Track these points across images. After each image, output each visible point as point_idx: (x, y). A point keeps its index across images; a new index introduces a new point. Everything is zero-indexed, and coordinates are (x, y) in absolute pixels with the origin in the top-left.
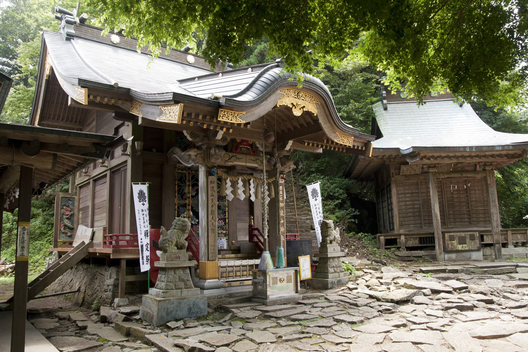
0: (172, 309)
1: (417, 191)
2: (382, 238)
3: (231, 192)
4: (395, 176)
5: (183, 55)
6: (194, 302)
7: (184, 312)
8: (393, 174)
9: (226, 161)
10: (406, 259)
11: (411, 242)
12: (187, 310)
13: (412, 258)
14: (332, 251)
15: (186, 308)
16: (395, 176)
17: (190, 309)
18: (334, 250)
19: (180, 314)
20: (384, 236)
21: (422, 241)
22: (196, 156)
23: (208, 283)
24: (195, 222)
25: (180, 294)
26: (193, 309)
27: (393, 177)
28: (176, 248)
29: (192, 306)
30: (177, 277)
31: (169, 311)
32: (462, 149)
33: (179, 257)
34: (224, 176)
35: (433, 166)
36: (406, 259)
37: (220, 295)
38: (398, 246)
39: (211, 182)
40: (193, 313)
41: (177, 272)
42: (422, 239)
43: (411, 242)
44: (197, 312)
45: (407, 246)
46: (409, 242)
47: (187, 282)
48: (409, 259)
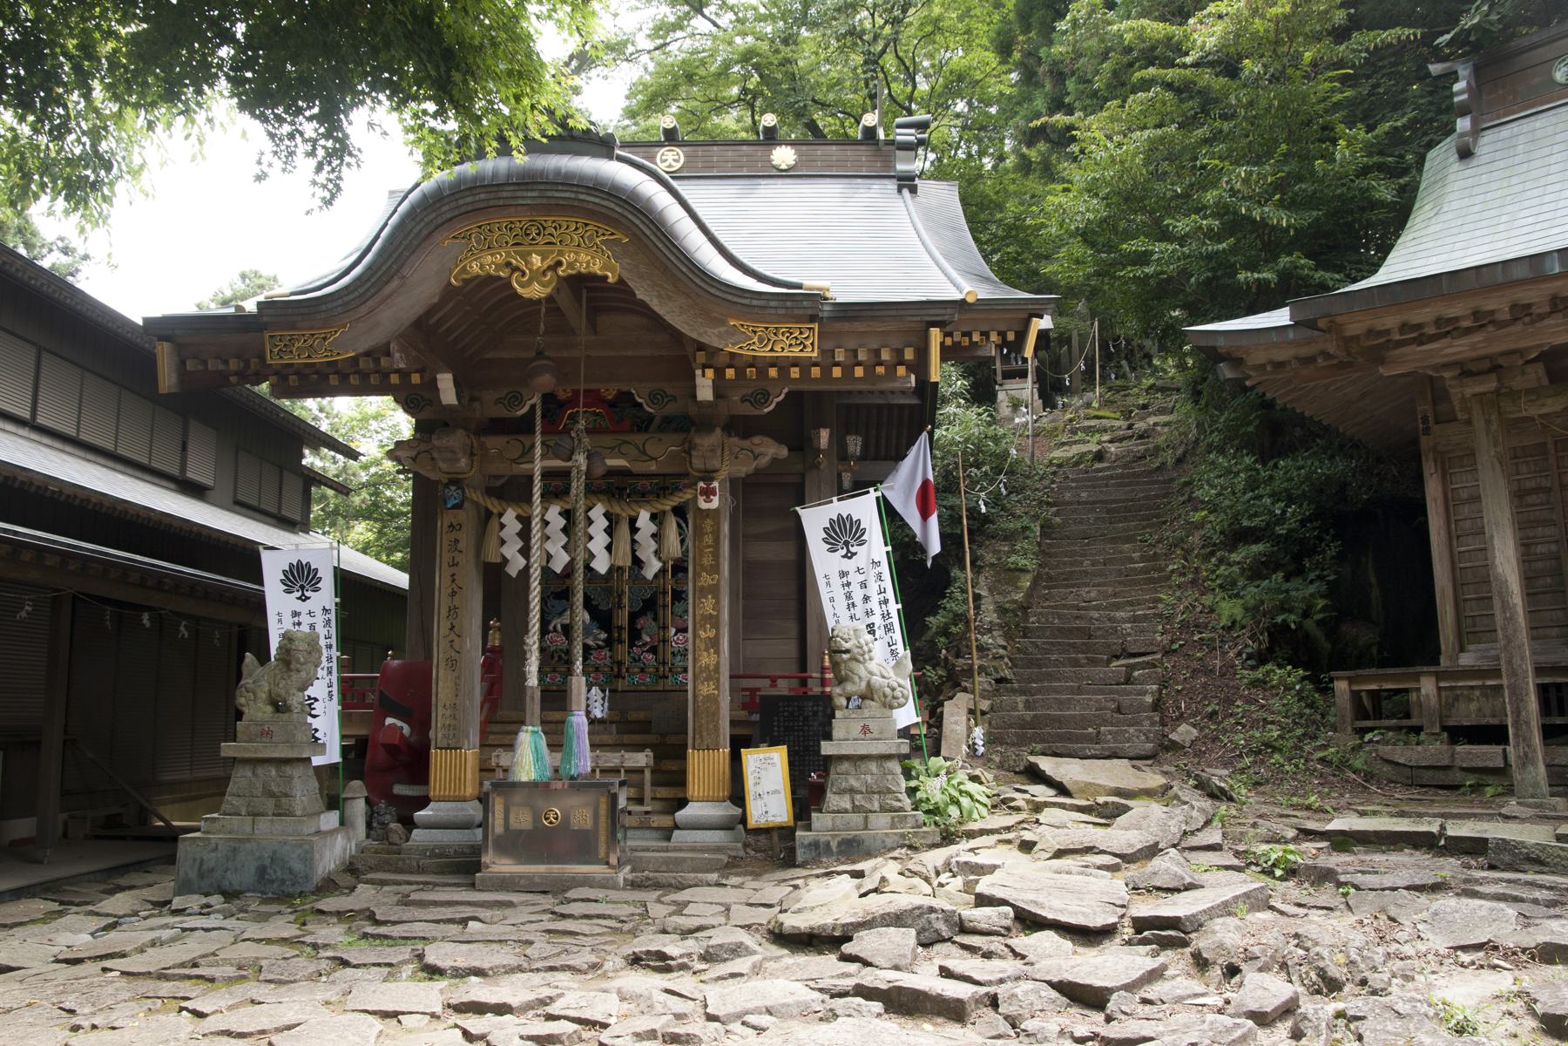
0: (212, 864)
1: (1546, 483)
2: (1341, 686)
3: (520, 551)
4: (1436, 429)
5: (759, 151)
6: (274, 852)
7: (243, 875)
8: (1425, 420)
9: (514, 461)
10: (1427, 776)
11: (1473, 706)
12: (253, 870)
13: (1458, 776)
14: (856, 729)
15: (251, 868)
16: (1436, 429)
17: (262, 871)
18: (865, 730)
19: (234, 880)
20: (1351, 681)
21: (1554, 704)
22: (414, 460)
23: (692, 811)
24: (596, 639)
25: (248, 829)
26: (270, 871)
27: (1427, 431)
28: (269, 709)
29: (267, 862)
30: (259, 785)
31: (205, 867)
32: (1519, 272)
33: (269, 733)
34: (493, 505)
35: (1486, 365)
36: (1427, 776)
37: (440, 847)
38: (1414, 722)
39: (451, 525)
40: (272, 882)
41: (260, 771)
42: (1553, 695)
43: (1473, 706)
44: (283, 881)
45: (1451, 722)
46: (1462, 706)
47: (283, 800)
48: (1442, 778)
